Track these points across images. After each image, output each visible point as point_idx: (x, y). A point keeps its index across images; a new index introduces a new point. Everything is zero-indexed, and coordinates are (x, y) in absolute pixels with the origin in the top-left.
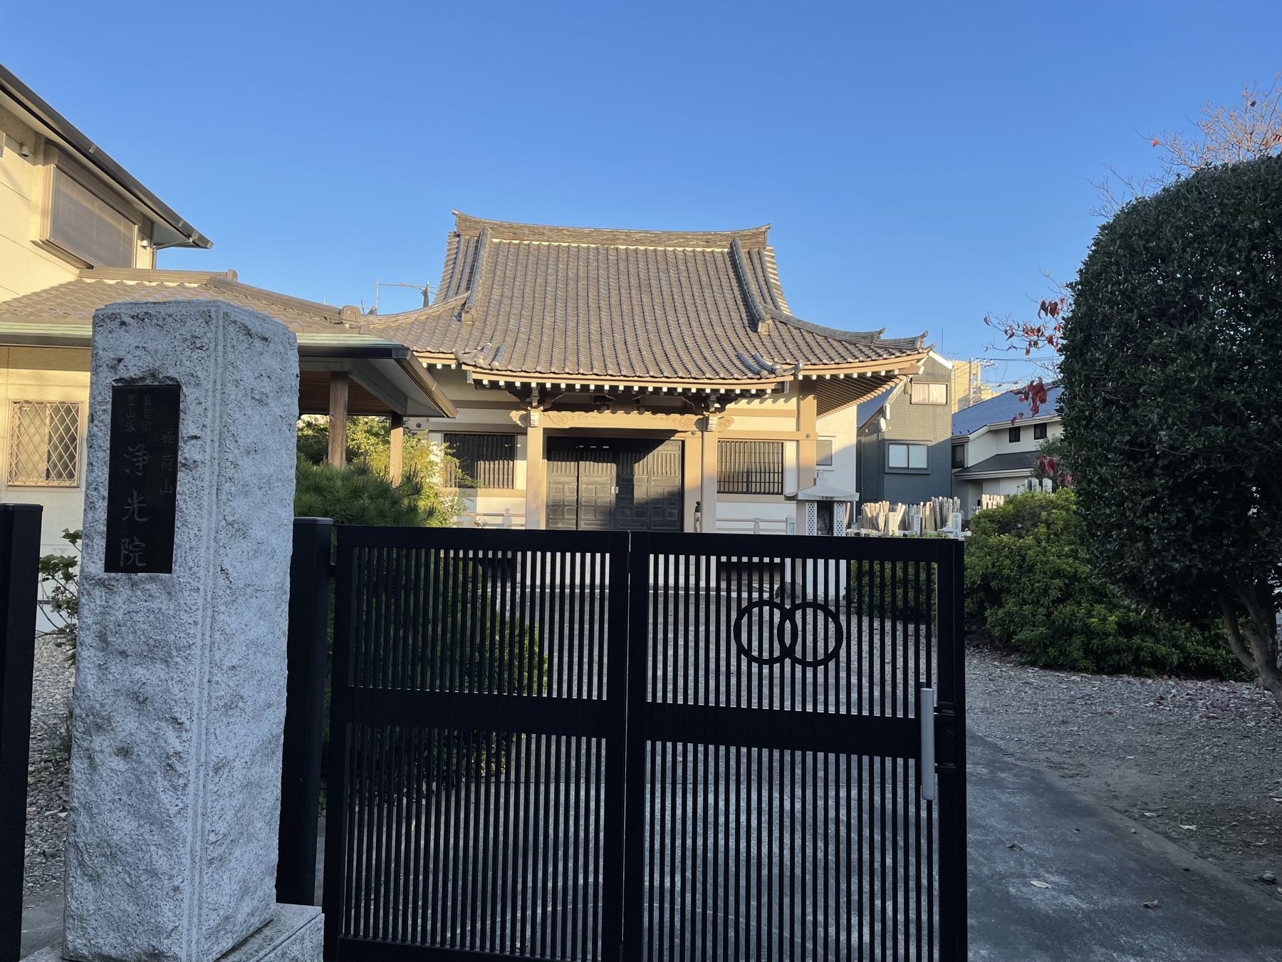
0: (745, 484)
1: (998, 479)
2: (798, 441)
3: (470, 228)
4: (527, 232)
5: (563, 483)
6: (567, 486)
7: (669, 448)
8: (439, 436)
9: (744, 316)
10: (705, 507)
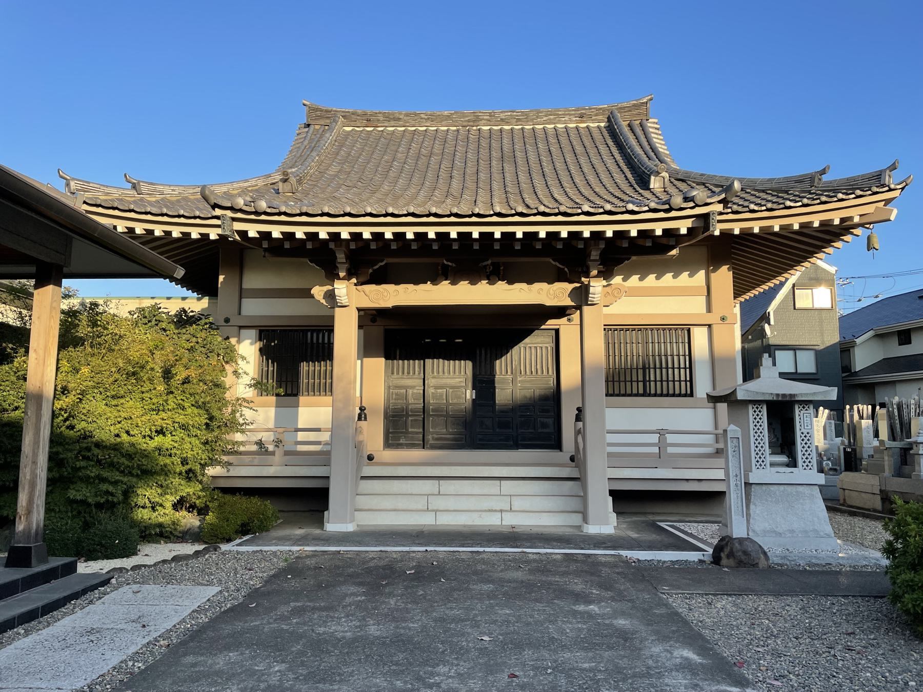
0: (641, 384)
1: (893, 383)
2: (710, 326)
3: (321, 117)
4: (381, 118)
5: (406, 388)
6: (410, 392)
7: (539, 340)
8: (253, 333)
9: (630, 176)
10: (588, 414)
